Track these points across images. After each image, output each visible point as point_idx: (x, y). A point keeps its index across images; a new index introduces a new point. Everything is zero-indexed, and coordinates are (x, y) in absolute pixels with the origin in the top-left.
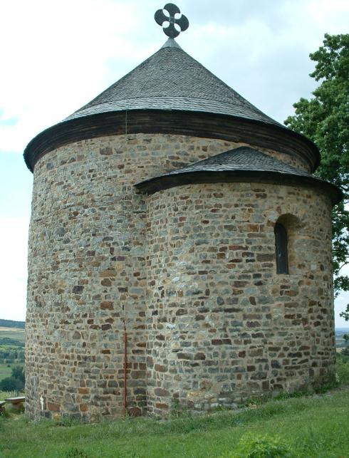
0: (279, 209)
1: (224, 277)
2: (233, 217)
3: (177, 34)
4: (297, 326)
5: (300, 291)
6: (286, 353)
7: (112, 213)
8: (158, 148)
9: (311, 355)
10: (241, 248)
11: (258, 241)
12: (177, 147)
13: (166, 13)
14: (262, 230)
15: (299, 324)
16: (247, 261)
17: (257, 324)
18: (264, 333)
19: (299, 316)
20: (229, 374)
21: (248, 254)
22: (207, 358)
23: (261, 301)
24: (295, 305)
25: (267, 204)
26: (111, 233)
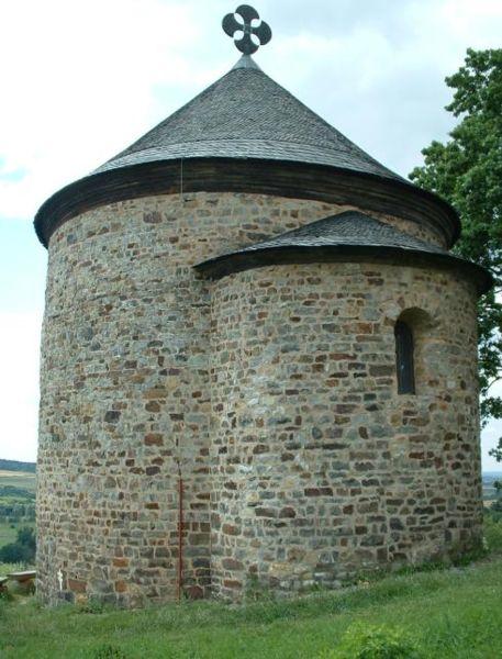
0: (401, 301)
1: (322, 399)
2: (336, 313)
4: (428, 469)
5: (432, 419)
6: (412, 508)
7: (160, 306)
8: (228, 212)
9: (447, 510)
10: (347, 356)
11: (371, 347)
12: (255, 212)
13: (239, 19)
14: (377, 331)
16: (356, 375)
17: (370, 466)
18: (380, 479)
19: (431, 454)
20: (329, 539)
21: (356, 366)
22: (298, 516)
23: (375, 433)
24: (425, 439)
25: (385, 294)
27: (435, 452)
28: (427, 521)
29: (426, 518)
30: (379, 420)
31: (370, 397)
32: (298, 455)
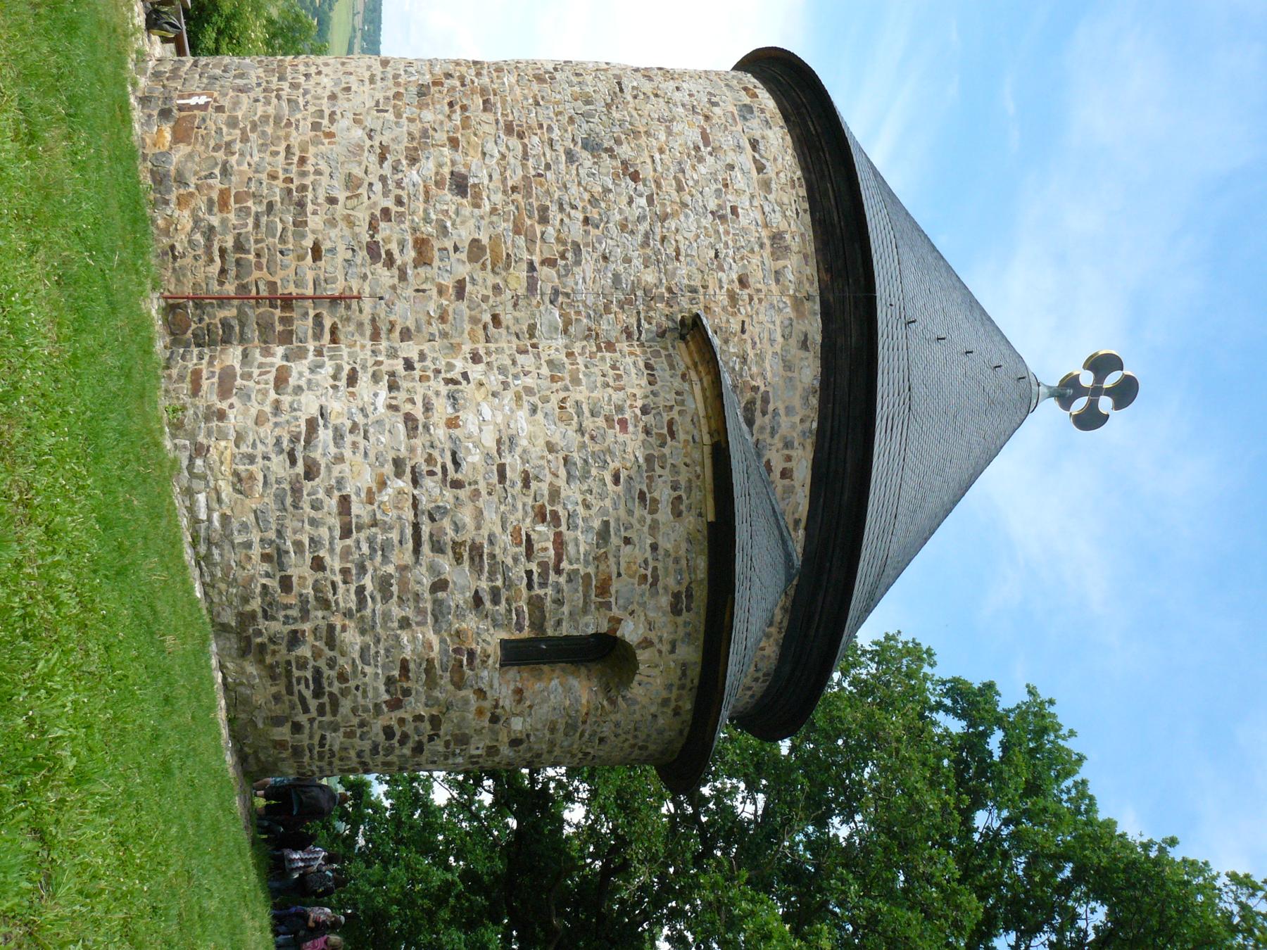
0: (647, 643)
2: (627, 541)
3: (1066, 402)
4: (382, 688)
5: (463, 693)
6: (322, 663)
10: (559, 559)
12: (789, 410)
15: (388, 691)
17: (387, 596)
19: (407, 692)
20: (272, 535)
21: (544, 575)
23: (437, 603)
24: (431, 682)
26: (589, 265)
27: (411, 699)
28: (302, 687)
29: (307, 686)
32: (404, 484)
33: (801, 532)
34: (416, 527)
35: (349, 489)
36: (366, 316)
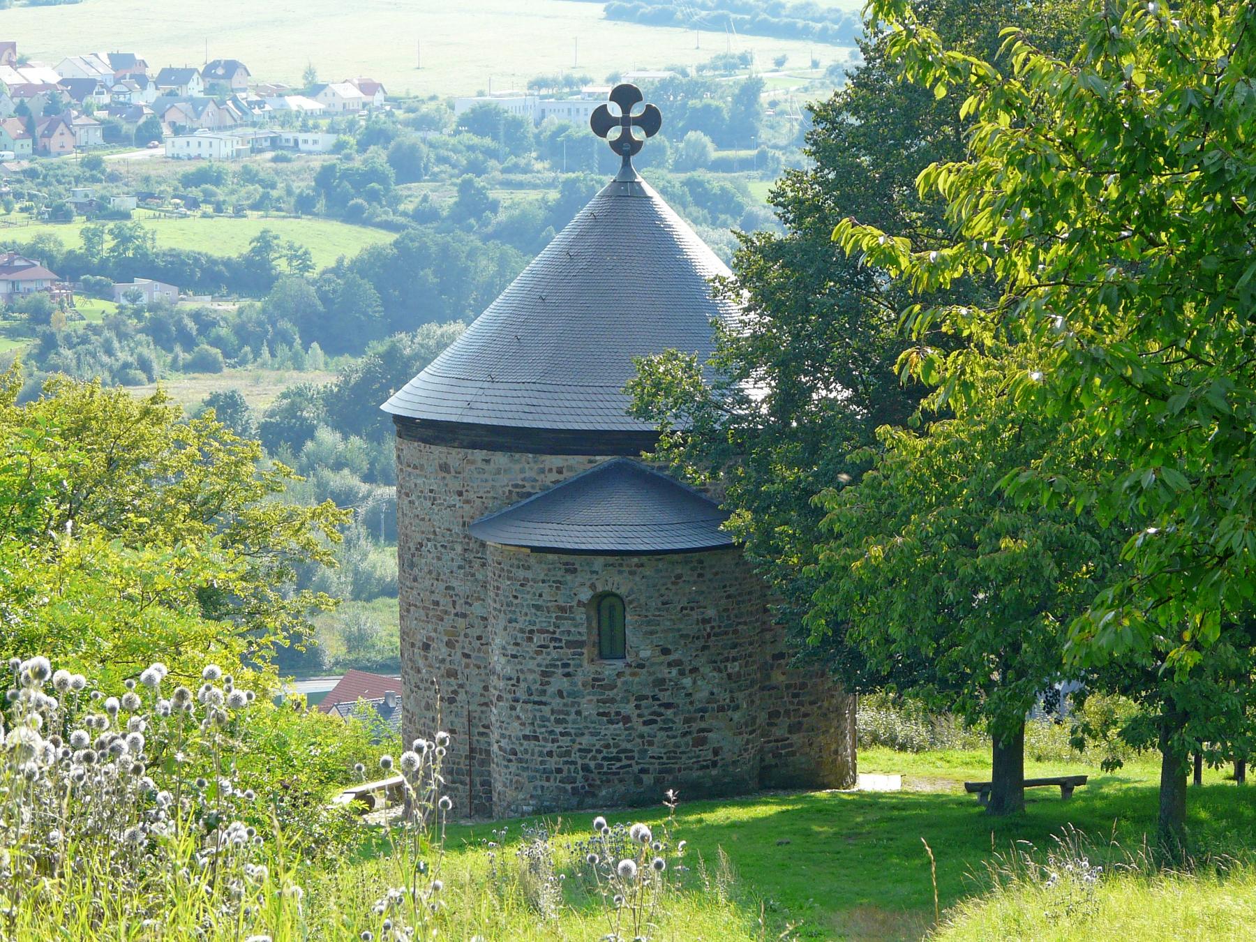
0: (593, 586)
1: (532, 665)
2: (540, 595)
5: (619, 684)
6: (600, 756)
7: (452, 554)
8: (498, 472)
10: (548, 632)
11: (566, 625)
12: (522, 471)
14: (571, 612)
16: (555, 648)
18: (573, 731)
19: (618, 713)
20: (538, 775)
21: (556, 640)
22: (519, 755)
23: (569, 695)
24: (613, 701)
30: (574, 684)
31: (566, 665)
33: (598, 458)
34: (535, 703)
35: (520, 734)
36: (479, 709)
